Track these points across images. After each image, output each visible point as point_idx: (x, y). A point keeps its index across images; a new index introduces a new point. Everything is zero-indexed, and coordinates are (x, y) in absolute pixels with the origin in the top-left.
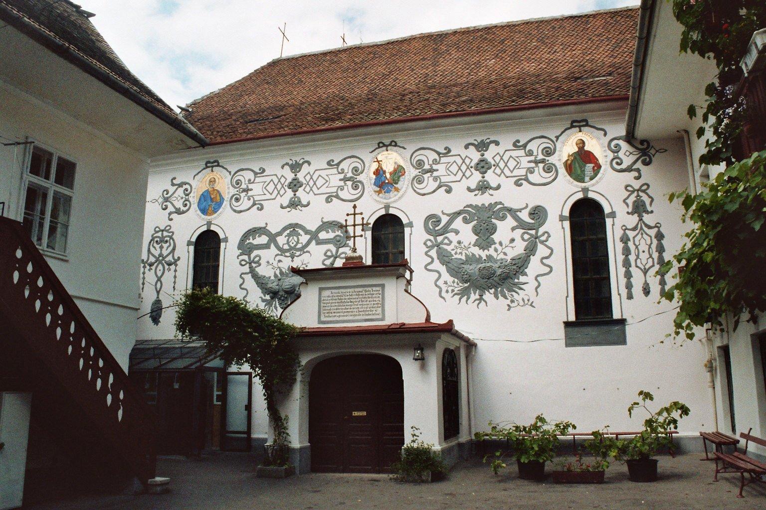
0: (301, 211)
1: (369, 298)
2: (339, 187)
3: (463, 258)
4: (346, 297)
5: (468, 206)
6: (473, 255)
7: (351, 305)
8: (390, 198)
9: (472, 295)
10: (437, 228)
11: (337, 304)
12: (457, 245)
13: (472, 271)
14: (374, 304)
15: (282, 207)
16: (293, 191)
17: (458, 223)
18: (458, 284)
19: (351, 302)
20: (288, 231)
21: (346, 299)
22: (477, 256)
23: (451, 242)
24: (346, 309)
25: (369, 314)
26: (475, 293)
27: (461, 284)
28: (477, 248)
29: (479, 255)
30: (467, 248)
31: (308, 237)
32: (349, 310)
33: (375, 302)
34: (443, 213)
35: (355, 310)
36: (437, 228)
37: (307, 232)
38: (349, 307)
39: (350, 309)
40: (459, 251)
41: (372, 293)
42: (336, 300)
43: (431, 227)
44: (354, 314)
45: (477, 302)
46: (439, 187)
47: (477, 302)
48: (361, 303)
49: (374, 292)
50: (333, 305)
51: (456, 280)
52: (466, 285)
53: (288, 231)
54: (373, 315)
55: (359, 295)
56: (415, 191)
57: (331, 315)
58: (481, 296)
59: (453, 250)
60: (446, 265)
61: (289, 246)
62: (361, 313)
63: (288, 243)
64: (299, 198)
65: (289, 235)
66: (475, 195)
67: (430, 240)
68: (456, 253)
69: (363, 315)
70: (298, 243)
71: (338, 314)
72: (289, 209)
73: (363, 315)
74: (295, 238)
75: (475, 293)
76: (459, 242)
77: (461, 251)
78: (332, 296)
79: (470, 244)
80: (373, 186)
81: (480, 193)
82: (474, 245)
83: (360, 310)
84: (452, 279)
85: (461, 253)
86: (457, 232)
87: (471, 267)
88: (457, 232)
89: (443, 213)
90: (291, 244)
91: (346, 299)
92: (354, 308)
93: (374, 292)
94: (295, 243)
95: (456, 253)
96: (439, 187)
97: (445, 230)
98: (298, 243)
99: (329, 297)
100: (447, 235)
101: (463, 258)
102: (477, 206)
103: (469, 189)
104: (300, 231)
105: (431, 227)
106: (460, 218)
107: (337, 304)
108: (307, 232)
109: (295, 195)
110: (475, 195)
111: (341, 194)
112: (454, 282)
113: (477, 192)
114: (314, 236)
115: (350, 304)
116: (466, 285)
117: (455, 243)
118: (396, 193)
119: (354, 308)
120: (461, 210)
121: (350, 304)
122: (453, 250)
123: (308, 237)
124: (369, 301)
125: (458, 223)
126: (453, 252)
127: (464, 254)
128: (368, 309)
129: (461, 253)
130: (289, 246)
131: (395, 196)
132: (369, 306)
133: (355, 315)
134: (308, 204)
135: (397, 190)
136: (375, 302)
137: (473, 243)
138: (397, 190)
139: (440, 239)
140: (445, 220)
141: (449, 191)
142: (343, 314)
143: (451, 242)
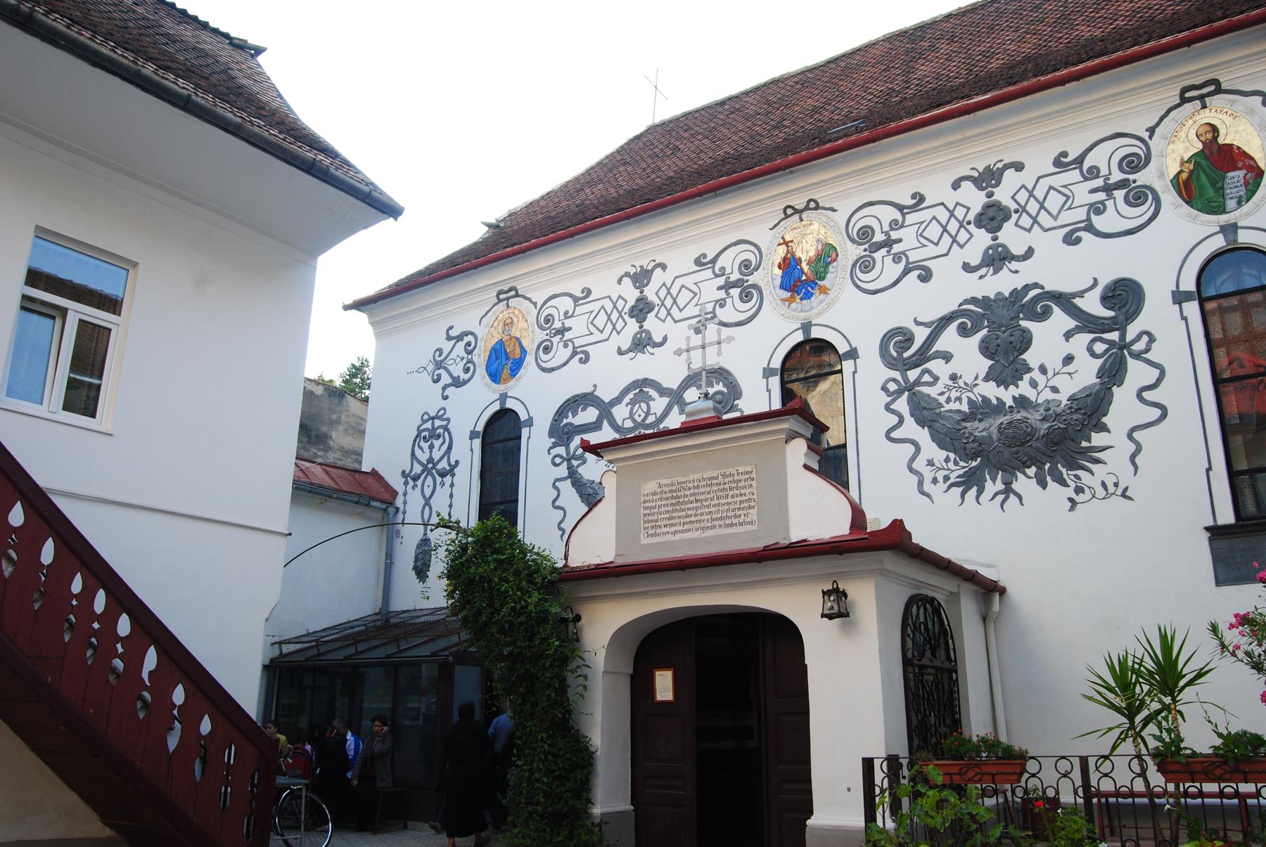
0: (1017, 272)
1: (731, 489)
2: (717, 301)
3: (965, 407)
4: (688, 493)
5: (966, 302)
6: (985, 400)
7: (697, 508)
8: (811, 308)
9: (989, 484)
10: (906, 355)
11: (670, 508)
12: (950, 383)
13: (984, 433)
14: (741, 502)
15: (620, 352)
16: (988, 231)
17: (949, 339)
18: (956, 463)
19: (697, 501)
20: (631, 395)
21: (685, 496)
22: (994, 402)
23: (936, 379)
24: (687, 516)
25: (732, 525)
26: (994, 480)
27: (962, 464)
28: (992, 384)
29: (998, 399)
30: (971, 387)
31: (666, 400)
32: (693, 519)
33: (743, 498)
34: (918, 323)
35: (705, 517)
36: (906, 355)
37: (662, 392)
38: (693, 512)
39: (696, 515)
40: (954, 394)
41: (736, 478)
42: (667, 499)
43: (895, 354)
44: (703, 525)
45: (1001, 497)
46: (906, 272)
47: (1001, 497)
48: (716, 502)
49: (741, 477)
50: (663, 509)
51: (952, 456)
52: (974, 464)
53: (631, 395)
54: (741, 524)
55: (711, 485)
56: (858, 287)
57: (659, 531)
58: (1008, 484)
59: (942, 394)
60: (929, 427)
61: (634, 421)
62: (716, 523)
63: (631, 417)
64: (648, 332)
65: (632, 403)
66: (981, 277)
67: (894, 380)
68: (948, 400)
69: (720, 526)
70: (648, 413)
71: (673, 529)
72: (631, 355)
73: (720, 526)
74: (644, 406)
75: (994, 480)
76: (954, 377)
77: (958, 394)
78: (661, 493)
79: (976, 378)
80: (778, 289)
81: (991, 271)
82: (986, 379)
83: (715, 516)
84: (944, 454)
85: (959, 399)
86: (947, 357)
87: (982, 426)
88: (947, 357)
89: (918, 323)
90: (636, 417)
91: (685, 496)
92: (702, 514)
93: (741, 477)
94: (643, 415)
95: (948, 400)
96: (906, 272)
97: (923, 356)
98: (648, 413)
99: (654, 494)
100: (928, 365)
101: (965, 407)
102: (986, 299)
103: (967, 268)
104: (652, 393)
105: (895, 354)
106: (953, 327)
107: (670, 508)
108: (662, 392)
109: (995, 239)
110: (981, 277)
111: (1098, 222)
112: (947, 460)
113: (983, 271)
114: (676, 397)
115: (695, 505)
116: (974, 464)
117: (944, 380)
118: (822, 296)
119: (702, 514)
120: (953, 313)
121: (695, 505)
122: (942, 394)
123: (666, 400)
124: (733, 497)
125: (949, 339)
126: (942, 399)
127: (965, 401)
128: (731, 514)
129: (959, 399)
130: (634, 421)
131: (821, 302)
132: (732, 507)
133: (704, 529)
134: (665, 339)
135: (824, 291)
136: (743, 498)
137: (982, 375)
138: (824, 291)
139: (913, 375)
140: (921, 335)
141: (926, 276)
142: (680, 528)
143: (936, 379)
